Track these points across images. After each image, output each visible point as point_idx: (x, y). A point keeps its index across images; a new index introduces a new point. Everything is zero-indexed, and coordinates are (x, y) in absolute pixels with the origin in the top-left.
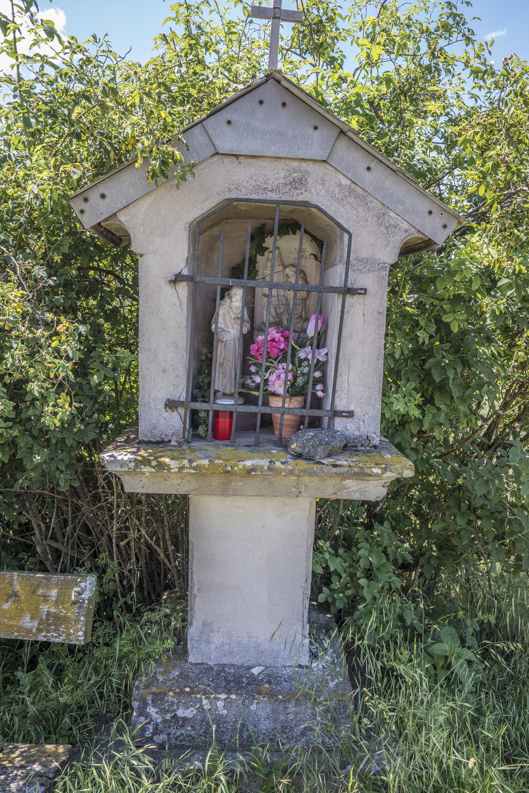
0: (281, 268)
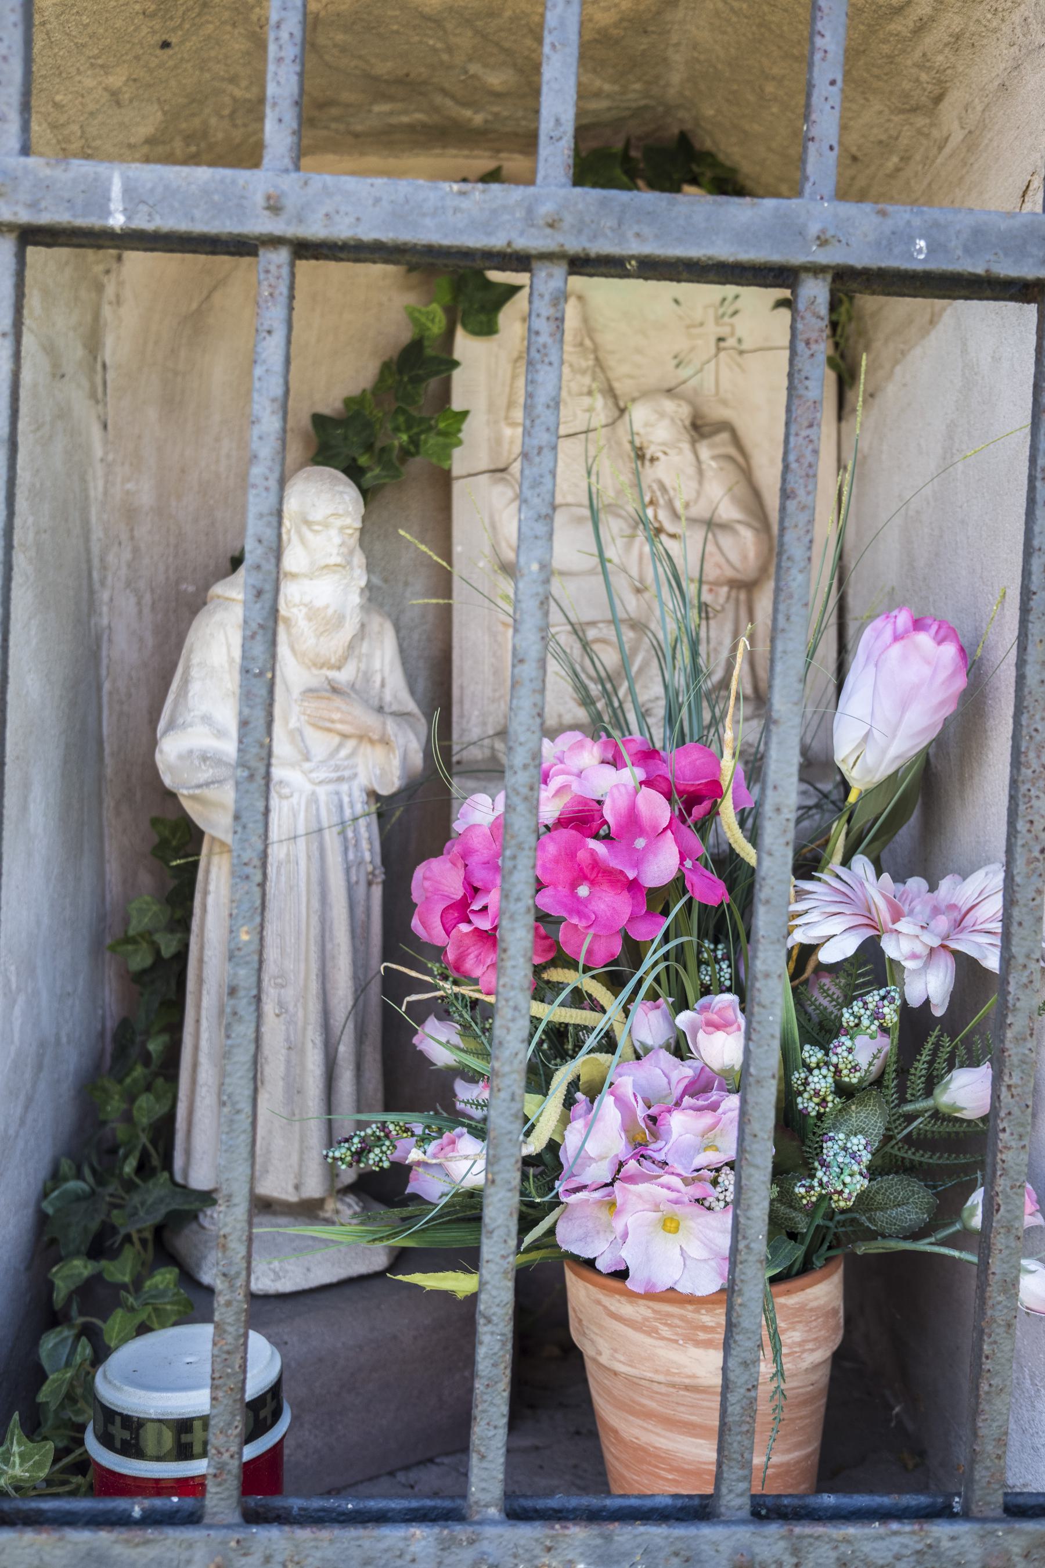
0: (601, 409)
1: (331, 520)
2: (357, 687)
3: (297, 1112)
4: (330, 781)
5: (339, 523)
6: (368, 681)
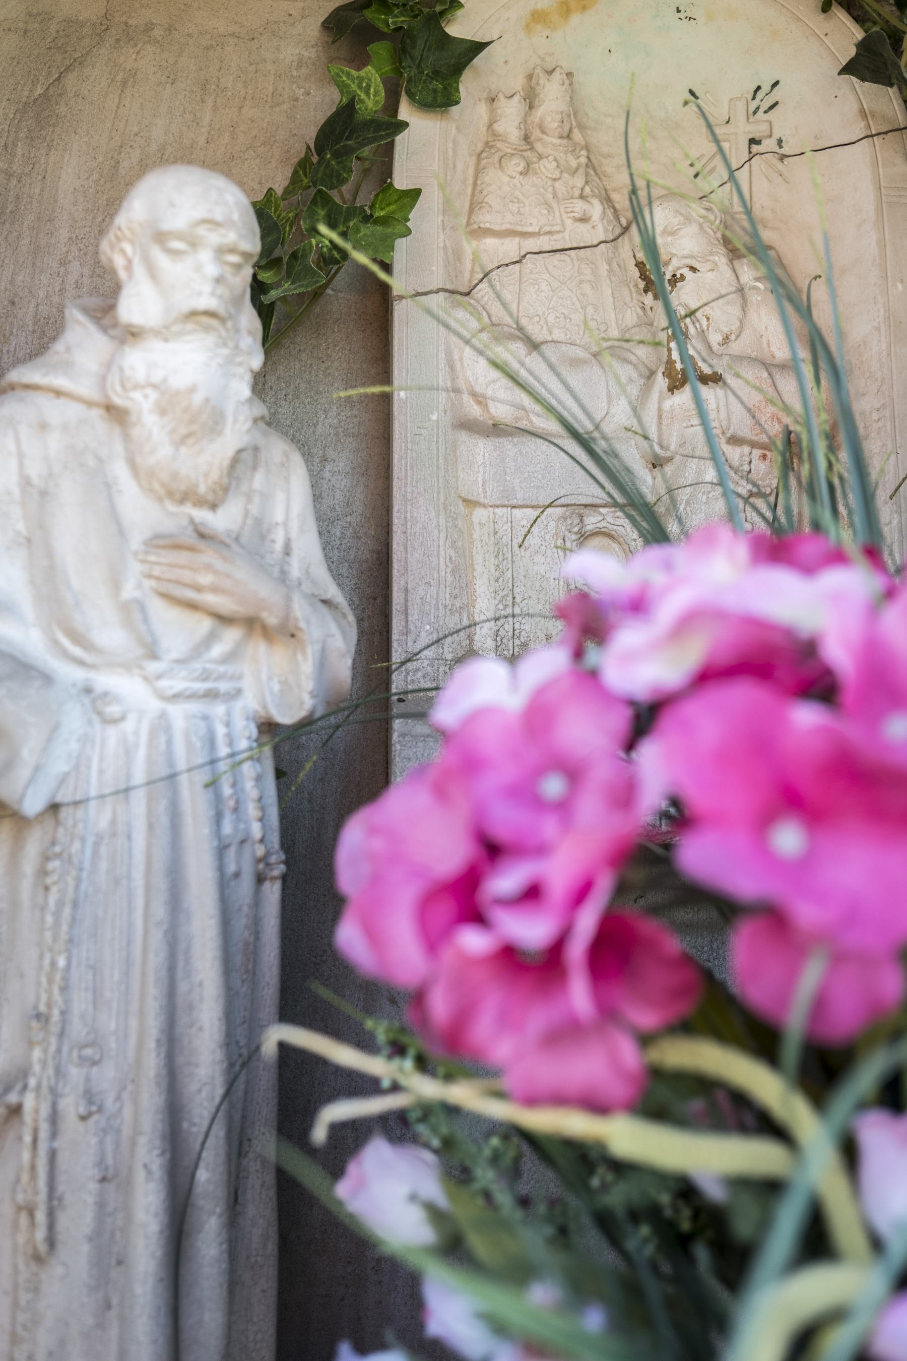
1: (202, 231)
2: (244, 540)
3: (115, 1301)
4: (193, 696)
5: (214, 238)
6: (263, 537)
